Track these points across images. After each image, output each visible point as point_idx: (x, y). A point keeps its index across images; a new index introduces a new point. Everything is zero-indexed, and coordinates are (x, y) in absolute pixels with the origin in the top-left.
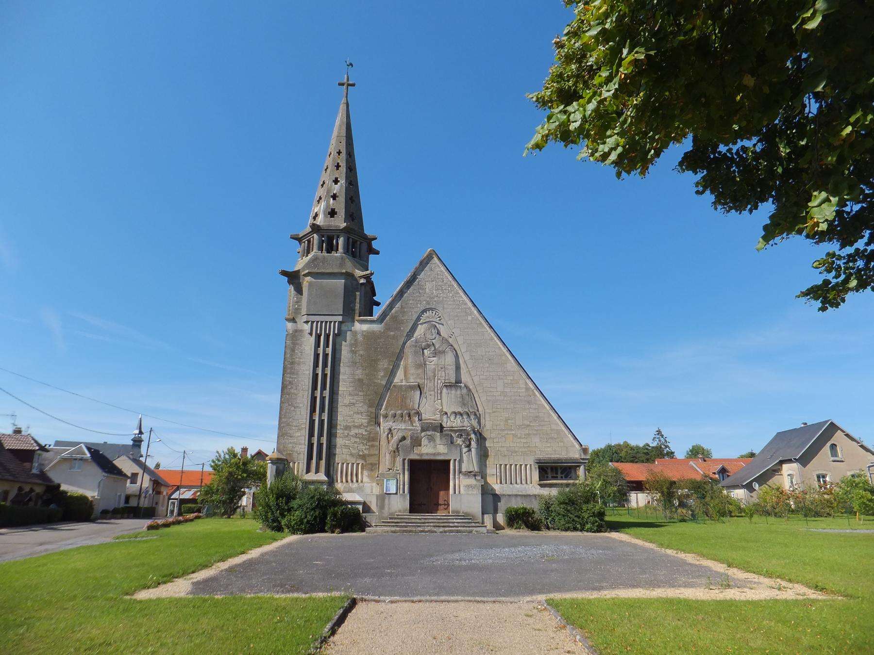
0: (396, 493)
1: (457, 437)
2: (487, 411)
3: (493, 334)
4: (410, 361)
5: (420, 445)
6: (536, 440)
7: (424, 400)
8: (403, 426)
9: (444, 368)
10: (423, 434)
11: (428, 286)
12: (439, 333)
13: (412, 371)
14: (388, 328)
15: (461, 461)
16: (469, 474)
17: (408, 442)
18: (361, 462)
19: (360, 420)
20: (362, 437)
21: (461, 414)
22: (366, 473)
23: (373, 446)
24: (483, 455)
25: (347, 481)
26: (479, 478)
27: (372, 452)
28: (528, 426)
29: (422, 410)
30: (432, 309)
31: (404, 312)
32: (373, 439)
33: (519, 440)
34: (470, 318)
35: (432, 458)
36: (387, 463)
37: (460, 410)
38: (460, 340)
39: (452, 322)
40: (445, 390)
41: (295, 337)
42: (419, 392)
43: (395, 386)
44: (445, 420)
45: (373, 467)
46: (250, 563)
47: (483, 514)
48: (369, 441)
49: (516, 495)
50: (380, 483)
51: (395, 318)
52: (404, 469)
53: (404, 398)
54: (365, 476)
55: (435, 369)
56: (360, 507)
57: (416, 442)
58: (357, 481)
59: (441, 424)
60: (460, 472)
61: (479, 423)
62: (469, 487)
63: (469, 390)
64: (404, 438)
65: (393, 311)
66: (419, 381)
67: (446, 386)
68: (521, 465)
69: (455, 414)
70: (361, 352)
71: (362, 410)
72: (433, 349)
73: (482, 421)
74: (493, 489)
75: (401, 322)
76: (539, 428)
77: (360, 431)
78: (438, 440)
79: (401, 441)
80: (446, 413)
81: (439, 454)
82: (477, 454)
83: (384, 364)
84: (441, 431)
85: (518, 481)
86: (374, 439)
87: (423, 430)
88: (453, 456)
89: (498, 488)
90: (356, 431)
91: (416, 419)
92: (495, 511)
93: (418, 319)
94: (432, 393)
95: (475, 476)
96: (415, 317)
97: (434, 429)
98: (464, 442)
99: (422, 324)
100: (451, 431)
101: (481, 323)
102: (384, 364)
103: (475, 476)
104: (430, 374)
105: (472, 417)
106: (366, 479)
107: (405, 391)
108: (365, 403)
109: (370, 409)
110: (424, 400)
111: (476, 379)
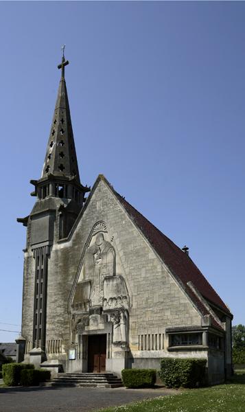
6: (168, 313)
11: (98, 204)
14: (74, 244)
23: (66, 328)
25: (142, 350)
28: (162, 302)
29: (92, 299)
30: (101, 222)
33: (155, 315)
37: (115, 296)
41: (27, 261)
42: (89, 287)
44: (105, 305)
49: (152, 359)
52: (80, 342)
60: (112, 342)
62: (117, 353)
66: (91, 278)
68: (146, 335)
69: (112, 299)
76: (170, 303)
80: (106, 299)
81: (99, 330)
85: (154, 348)
90: (58, 319)
93: (92, 231)
104: (97, 271)
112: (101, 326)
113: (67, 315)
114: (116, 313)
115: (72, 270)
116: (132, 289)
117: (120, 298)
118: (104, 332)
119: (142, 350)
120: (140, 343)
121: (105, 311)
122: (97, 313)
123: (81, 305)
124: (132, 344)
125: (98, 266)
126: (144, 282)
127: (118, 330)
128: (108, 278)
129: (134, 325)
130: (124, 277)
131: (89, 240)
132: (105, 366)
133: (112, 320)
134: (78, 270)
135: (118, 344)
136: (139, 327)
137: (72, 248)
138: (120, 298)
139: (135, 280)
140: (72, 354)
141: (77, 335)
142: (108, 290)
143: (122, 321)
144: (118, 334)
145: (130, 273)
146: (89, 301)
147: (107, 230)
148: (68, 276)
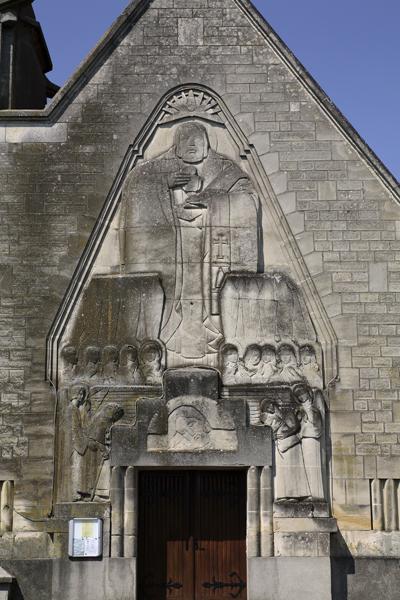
7: (176, 316)
9: (227, 235)
11: (184, 29)
14: (76, 137)
23: (39, 436)
29: (169, 339)
35: (196, 463)
37: (270, 340)
42: (160, 297)
44: (230, 366)
62: (295, 537)
66: (160, 267)
71: (12, 345)
78: (213, 420)
80: (234, 349)
81: (216, 452)
93: (157, 111)
96: (149, 106)
109: (31, 342)
111: (313, 262)
112: (223, 440)
113: (41, 388)
114: (288, 400)
115: (67, 227)
117: (291, 349)
118: (237, 463)
119: (383, 529)
120: (376, 504)
121: (234, 389)
122: (205, 394)
123: (116, 357)
124: (346, 508)
125: (190, 232)
126: (383, 309)
127: (296, 456)
128: (242, 278)
129: (347, 443)
131: (144, 138)
132: (243, 585)
133: (271, 419)
134: (97, 229)
135: (297, 505)
136: (370, 454)
137: (64, 151)
138: (291, 349)
139: (349, 299)
141: (105, 468)
142: (243, 318)
143: (309, 428)
144: (293, 468)
145: (325, 274)
146: (157, 348)
148: (47, 243)
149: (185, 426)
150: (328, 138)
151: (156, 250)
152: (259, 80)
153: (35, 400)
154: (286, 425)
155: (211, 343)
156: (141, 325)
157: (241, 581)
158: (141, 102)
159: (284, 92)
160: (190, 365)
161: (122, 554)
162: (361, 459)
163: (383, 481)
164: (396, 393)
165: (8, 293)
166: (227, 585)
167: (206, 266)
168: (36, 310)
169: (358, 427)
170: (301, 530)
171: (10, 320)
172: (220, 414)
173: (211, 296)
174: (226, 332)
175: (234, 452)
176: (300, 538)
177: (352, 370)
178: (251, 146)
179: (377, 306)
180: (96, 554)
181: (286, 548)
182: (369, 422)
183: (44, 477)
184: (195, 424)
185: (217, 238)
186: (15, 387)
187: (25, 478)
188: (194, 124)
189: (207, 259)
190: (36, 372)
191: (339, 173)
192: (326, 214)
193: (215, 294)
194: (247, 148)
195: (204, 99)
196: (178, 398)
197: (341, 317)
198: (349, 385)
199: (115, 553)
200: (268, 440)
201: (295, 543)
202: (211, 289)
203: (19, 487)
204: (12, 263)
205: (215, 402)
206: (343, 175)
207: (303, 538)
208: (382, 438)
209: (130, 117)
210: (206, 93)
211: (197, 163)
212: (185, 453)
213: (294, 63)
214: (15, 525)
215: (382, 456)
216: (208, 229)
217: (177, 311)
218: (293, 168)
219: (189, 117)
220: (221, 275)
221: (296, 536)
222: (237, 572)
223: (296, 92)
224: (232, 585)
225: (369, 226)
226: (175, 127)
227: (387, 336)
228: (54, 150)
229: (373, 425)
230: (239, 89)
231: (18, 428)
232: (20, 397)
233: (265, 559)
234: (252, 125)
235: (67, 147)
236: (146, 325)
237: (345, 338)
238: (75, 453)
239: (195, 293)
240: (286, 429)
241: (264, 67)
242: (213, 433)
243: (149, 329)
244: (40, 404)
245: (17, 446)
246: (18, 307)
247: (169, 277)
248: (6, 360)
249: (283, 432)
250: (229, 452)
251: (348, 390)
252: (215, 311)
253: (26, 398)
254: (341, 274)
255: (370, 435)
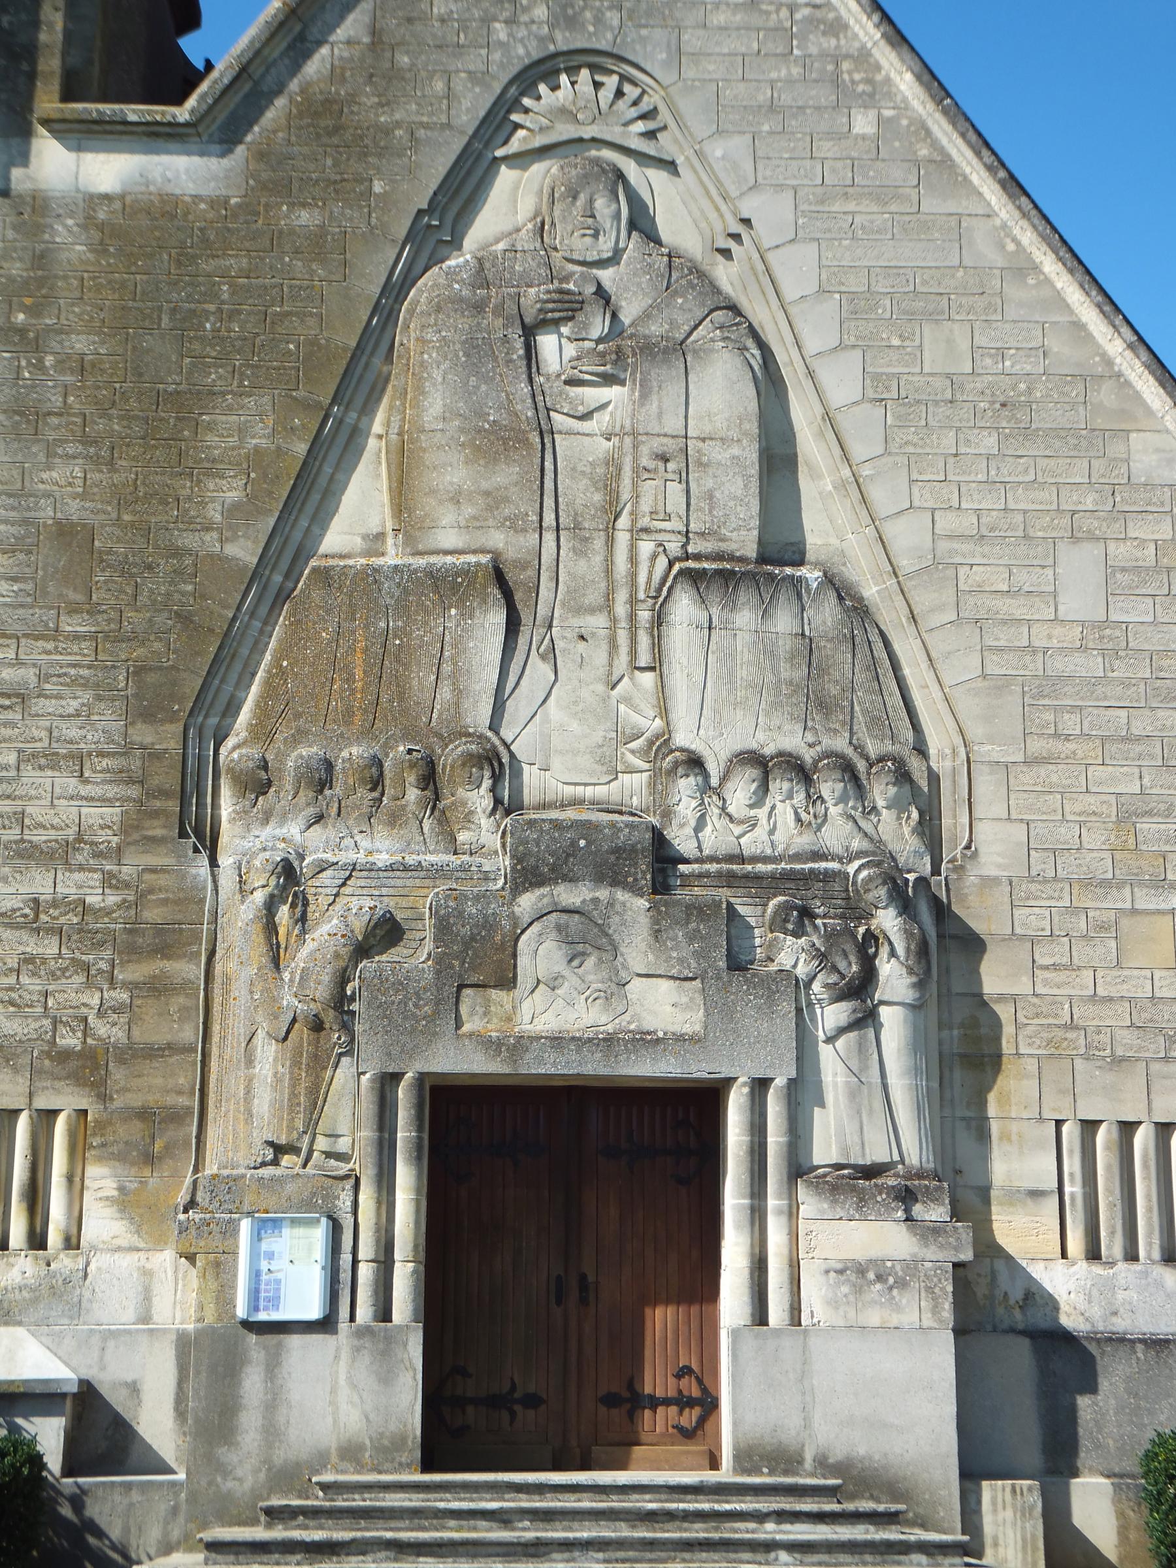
0: (326, 1325)
1: (779, 923)
2: (986, 751)
3: (1027, 236)
4: (434, 405)
5: (507, 981)
7: (539, 670)
8: (381, 847)
9: (678, 458)
10: (527, 902)
12: (641, 222)
13: (450, 471)
14: (275, 181)
15: (803, 1092)
16: (859, 1182)
17: (417, 956)
18: (67, 1100)
19: (68, 811)
20: (80, 927)
21: (802, 772)
22: (101, 1179)
23: (157, 988)
24: (964, 1055)
25: (1093, 1254)
26: (935, 1213)
27: (156, 1029)
29: (521, 737)
30: (595, 60)
31: (395, 75)
32: (160, 940)
34: (863, 124)
35: (593, 1066)
36: (264, 1102)
38: (797, 271)
39: (738, 145)
40: (684, 607)
42: (497, 618)
43: (324, 576)
45: (158, 1136)
46: (113, 1483)
47: (972, 1472)
48: (131, 951)
50: (206, 1251)
51: (326, 116)
53: (390, 660)
54: (98, 1206)
55: (613, 463)
56: (49, 1435)
57: (481, 958)
58: (37, 1241)
59: (659, 839)
60: (798, 1169)
61: (930, 830)
62: (861, 1274)
63: (857, 610)
64: (386, 932)
65: (316, 66)
66: (497, 539)
67: (695, 578)
68: (1127, 1128)
70: (81, 344)
71: (89, 738)
72: (598, 326)
73: (953, 821)
74: (1035, 1297)
75: (372, 145)
77: (69, 885)
78: (637, 950)
79: (362, 950)
80: (695, 763)
81: (646, 1041)
82: (918, 1043)
83: (249, 427)
84: (661, 886)
86: (166, 942)
87: (528, 874)
88: (745, 1056)
89: (1073, 1290)
91: (480, 799)
92: (1059, 1459)
93: (497, 121)
94: (597, 622)
95: (907, 1197)
96: (471, 107)
97: (611, 868)
98: (822, 957)
99: (522, 159)
100: (730, 880)
101: (945, 162)
102: (249, 427)
103: (907, 1197)
105: (881, 792)
106: (101, 1224)
107: (402, 608)
108: (103, 691)
109: (143, 734)
110: (539, 670)
111: (909, 537)
116: (967, 706)
125: (583, 445)
126: (1094, 665)
130: (870, 591)
140: (292, 1270)
145: (938, 567)
147: (666, 146)
149: (561, 967)
150: (951, 206)
151: (487, 493)
152: (770, 47)
153: (151, 891)
154: (835, 969)
155: (634, 745)
156: (445, 693)
157: (704, 1390)
158: (449, 94)
159: (836, 81)
160: (576, 802)
161: (760, 1317)
162: (1031, 1065)
163: (1090, 1127)
164: (1127, 891)
165: (80, 597)
166: (667, 1402)
167: (622, 539)
168: (157, 646)
169: (1026, 980)
170: (874, 1253)
171: (85, 672)
172: (657, 934)
173: (632, 617)
174: (673, 716)
175: (694, 1039)
176: (871, 1276)
177: (1008, 825)
178: (746, 222)
179: (1079, 658)
180: (314, 1312)
181: (833, 1303)
182: (1055, 967)
183: (170, 1100)
184: (591, 962)
185: (651, 465)
186: (98, 855)
187: (118, 1102)
188: (597, 162)
189: (623, 522)
190: (155, 814)
191: (980, 302)
192: (942, 410)
193: (644, 615)
194: (737, 228)
195: (619, 93)
196: (545, 890)
197: (980, 683)
198: (999, 866)
199: (364, 1312)
200: (787, 1007)
201: (858, 1290)
202: (633, 601)
203: (101, 1126)
204: (94, 520)
205: (642, 903)
206: (989, 307)
207: (880, 1278)
208: (1091, 1010)
209: (421, 133)
210: (624, 78)
211: (601, 263)
212: (557, 1041)
213: (714, 192)
214: (90, 1232)
215: (1087, 1058)
216: (628, 440)
217: (543, 657)
218: (855, 283)
219: (581, 140)
220: (662, 562)
221: (861, 1270)
222: (694, 1366)
223: (869, 81)
224: (683, 1402)
225: (1058, 443)
226: (538, 168)
227: (1104, 740)
228: (211, 215)
229: (1062, 976)
230: (712, 68)
231: (103, 965)
232: (110, 881)
233: (777, 1332)
234: (748, 166)
235: (248, 209)
236: (459, 693)
237: (991, 740)
238: (261, 1034)
239: (592, 610)
240: (833, 978)
241: (784, 13)
242: (636, 985)
243: (466, 704)
244: (165, 901)
245: (100, 1014)
246: (106, 638)
247: (524, 566)
248: (73, 782)
249: (826, 986)
250: (680, 1038)
251: (994, 881)
252: (644, 659)
253: (127, 886)
254: (985, 571)
255: (1054, 1001)
